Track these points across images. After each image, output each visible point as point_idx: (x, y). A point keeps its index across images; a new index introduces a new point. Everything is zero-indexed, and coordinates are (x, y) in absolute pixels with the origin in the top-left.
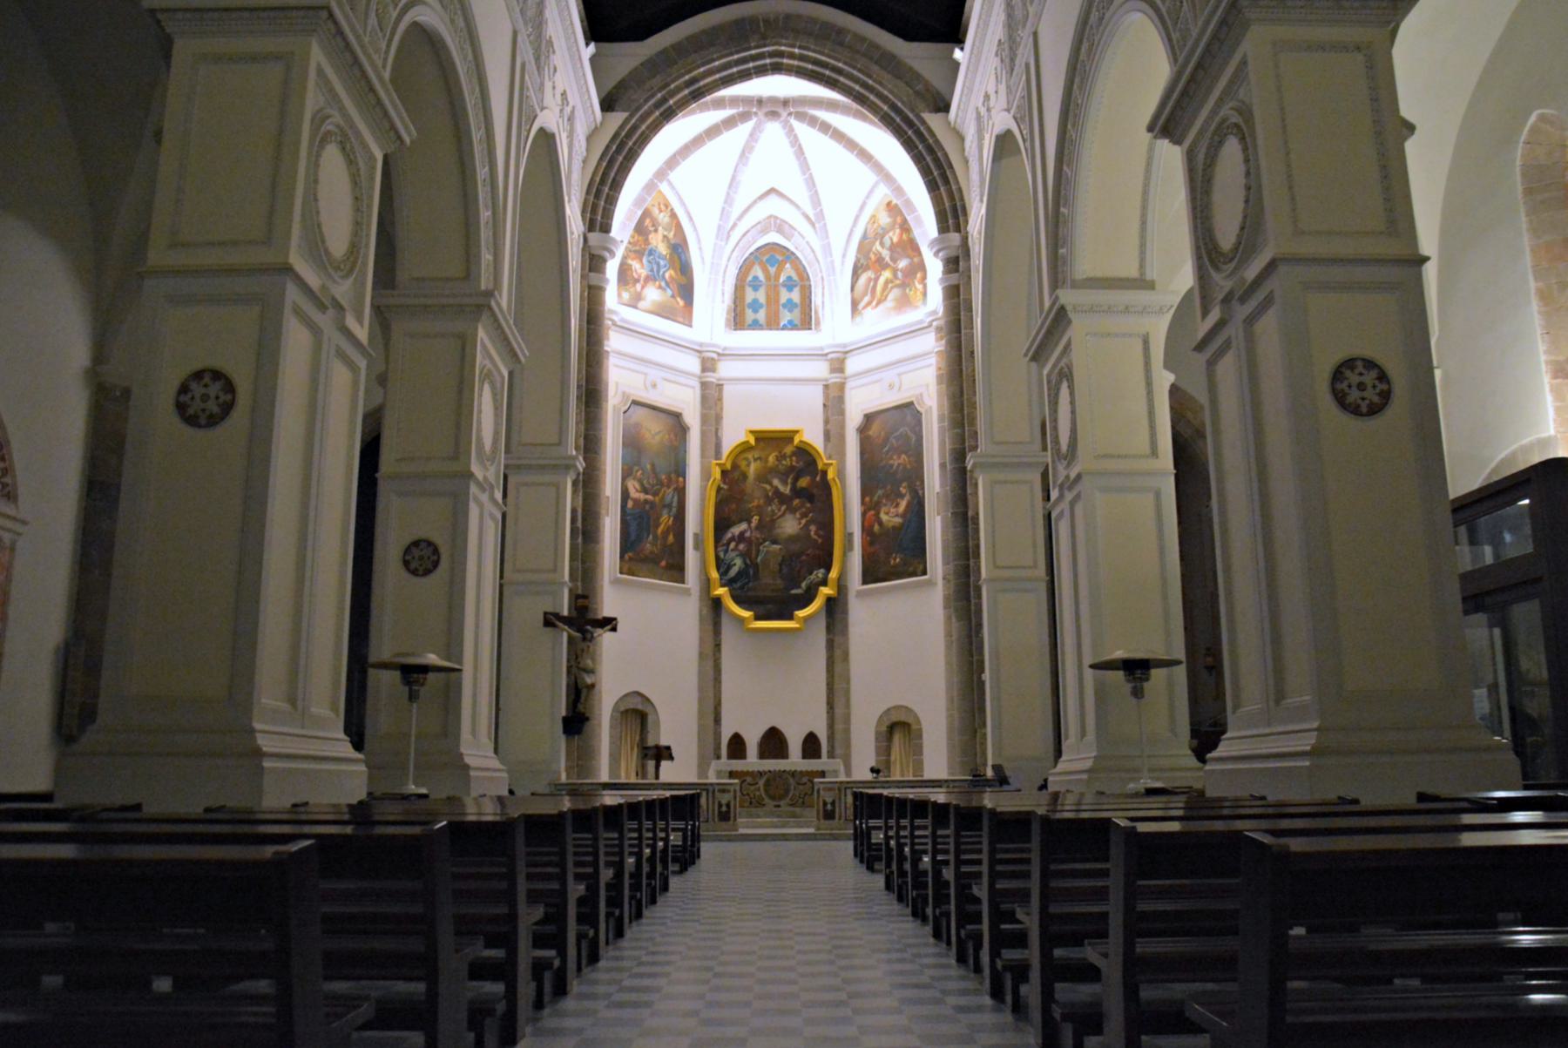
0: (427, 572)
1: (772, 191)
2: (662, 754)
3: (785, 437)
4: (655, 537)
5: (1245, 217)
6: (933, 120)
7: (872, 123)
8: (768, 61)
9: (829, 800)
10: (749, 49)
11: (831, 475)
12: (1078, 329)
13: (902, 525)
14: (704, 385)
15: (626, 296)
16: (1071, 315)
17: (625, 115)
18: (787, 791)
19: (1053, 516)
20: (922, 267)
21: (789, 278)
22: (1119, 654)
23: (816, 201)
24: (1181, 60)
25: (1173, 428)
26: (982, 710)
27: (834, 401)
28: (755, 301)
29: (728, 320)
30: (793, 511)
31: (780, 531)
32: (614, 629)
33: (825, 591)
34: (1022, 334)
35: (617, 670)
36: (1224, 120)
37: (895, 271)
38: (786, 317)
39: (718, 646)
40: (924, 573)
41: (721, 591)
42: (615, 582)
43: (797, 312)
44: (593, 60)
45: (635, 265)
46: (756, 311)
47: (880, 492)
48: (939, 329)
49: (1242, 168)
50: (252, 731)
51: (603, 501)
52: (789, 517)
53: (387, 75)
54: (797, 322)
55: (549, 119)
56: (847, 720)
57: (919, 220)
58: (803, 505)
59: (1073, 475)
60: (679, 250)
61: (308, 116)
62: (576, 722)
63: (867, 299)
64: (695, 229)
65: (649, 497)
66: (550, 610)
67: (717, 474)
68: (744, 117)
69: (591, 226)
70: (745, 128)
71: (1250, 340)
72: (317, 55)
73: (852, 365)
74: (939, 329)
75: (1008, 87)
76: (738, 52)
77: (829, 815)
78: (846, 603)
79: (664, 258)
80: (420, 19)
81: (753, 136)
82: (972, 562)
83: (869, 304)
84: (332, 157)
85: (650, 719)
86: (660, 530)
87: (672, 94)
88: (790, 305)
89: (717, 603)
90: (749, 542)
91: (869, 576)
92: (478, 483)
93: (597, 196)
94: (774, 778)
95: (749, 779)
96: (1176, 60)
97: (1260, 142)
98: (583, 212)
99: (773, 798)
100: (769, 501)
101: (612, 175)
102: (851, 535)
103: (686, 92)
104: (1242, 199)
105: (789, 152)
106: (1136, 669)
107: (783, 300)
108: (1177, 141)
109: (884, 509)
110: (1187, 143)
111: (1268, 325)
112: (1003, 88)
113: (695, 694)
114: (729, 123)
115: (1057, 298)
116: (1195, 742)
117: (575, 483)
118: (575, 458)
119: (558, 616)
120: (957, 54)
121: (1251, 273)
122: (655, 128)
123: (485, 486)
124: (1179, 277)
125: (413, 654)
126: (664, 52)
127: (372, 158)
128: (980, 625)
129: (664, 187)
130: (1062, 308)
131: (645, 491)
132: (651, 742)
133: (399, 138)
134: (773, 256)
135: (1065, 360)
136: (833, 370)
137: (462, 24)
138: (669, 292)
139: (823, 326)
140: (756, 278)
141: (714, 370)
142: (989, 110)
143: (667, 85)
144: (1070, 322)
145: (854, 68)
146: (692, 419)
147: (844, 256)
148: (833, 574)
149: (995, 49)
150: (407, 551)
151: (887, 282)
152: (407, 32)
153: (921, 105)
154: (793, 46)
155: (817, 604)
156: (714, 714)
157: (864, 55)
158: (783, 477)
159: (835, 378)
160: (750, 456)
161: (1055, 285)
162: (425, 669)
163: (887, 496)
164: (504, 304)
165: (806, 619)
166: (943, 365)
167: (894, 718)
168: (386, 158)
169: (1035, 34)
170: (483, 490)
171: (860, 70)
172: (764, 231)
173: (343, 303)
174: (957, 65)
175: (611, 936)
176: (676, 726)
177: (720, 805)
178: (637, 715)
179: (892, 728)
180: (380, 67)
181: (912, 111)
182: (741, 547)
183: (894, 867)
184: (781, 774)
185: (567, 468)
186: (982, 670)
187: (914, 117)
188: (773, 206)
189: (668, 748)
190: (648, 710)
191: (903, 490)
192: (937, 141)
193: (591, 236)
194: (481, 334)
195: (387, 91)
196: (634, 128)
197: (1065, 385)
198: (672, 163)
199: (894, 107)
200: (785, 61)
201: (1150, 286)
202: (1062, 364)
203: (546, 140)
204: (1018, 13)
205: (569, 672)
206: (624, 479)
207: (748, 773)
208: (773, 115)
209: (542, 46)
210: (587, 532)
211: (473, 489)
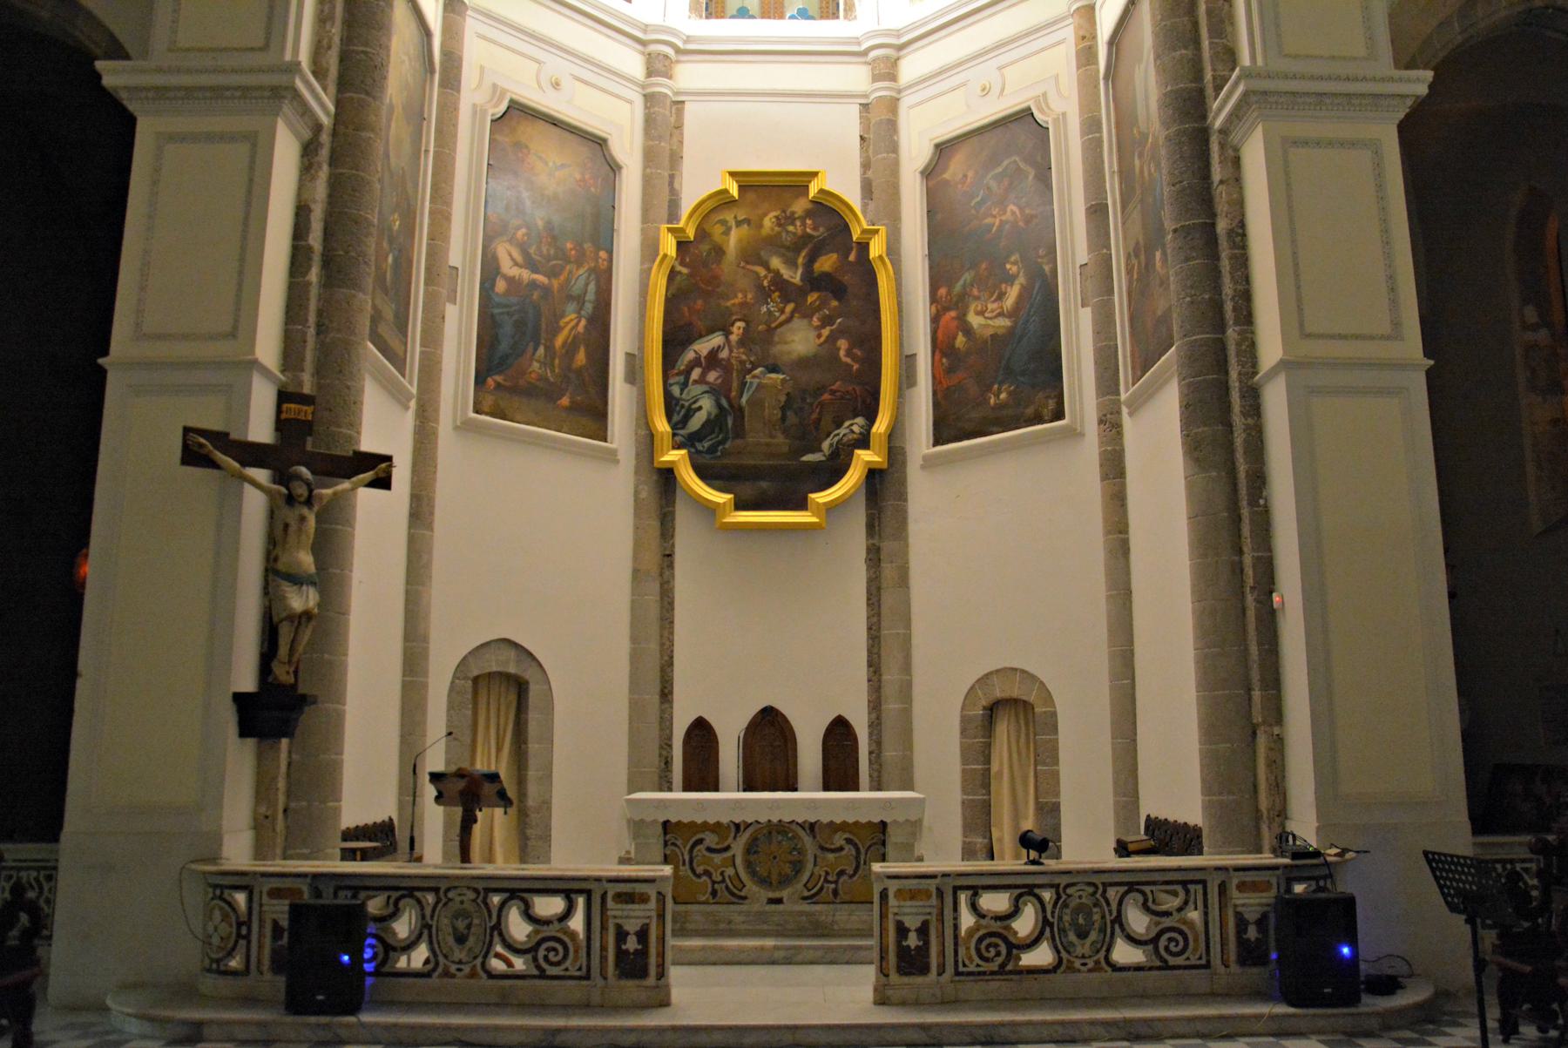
3: (796, 183)
4: (550, 349)
9: (912, 923)
11: (876, 249)
13: (1011, 332)
14: (650, 99)
18: (798, 867)
27: (880, 129)
30: (808, 316)
33: (865, 457)
40: (1059, 415)
41: (675, 457)
42: (465, 427)
47: (967, 277)
52: (797, 323)
58: (824, 303)
67: (669, 246)
73: (912, 67)
77: (912, 962)
78: (903, 482)
82: (1232, 333)
85: (534, 690)
86: (559, 340)
89: (667, 476)
90: (726, 367)
91: (941, 435)
94: (769, 838)
95: (711, 840)
99: (764, 882)
100: (764, 294)
102: (911, 358)
113: (623, 647)
146: (628, 149)
148: (881, 426)
155: (851, 480)
159: (882, 90)
160: (729, 216)
165: (831, 508)
177: (621, 935)
179: (992, 710)
182: (712, 376)
184: (779, 830)
190: (529, 674)
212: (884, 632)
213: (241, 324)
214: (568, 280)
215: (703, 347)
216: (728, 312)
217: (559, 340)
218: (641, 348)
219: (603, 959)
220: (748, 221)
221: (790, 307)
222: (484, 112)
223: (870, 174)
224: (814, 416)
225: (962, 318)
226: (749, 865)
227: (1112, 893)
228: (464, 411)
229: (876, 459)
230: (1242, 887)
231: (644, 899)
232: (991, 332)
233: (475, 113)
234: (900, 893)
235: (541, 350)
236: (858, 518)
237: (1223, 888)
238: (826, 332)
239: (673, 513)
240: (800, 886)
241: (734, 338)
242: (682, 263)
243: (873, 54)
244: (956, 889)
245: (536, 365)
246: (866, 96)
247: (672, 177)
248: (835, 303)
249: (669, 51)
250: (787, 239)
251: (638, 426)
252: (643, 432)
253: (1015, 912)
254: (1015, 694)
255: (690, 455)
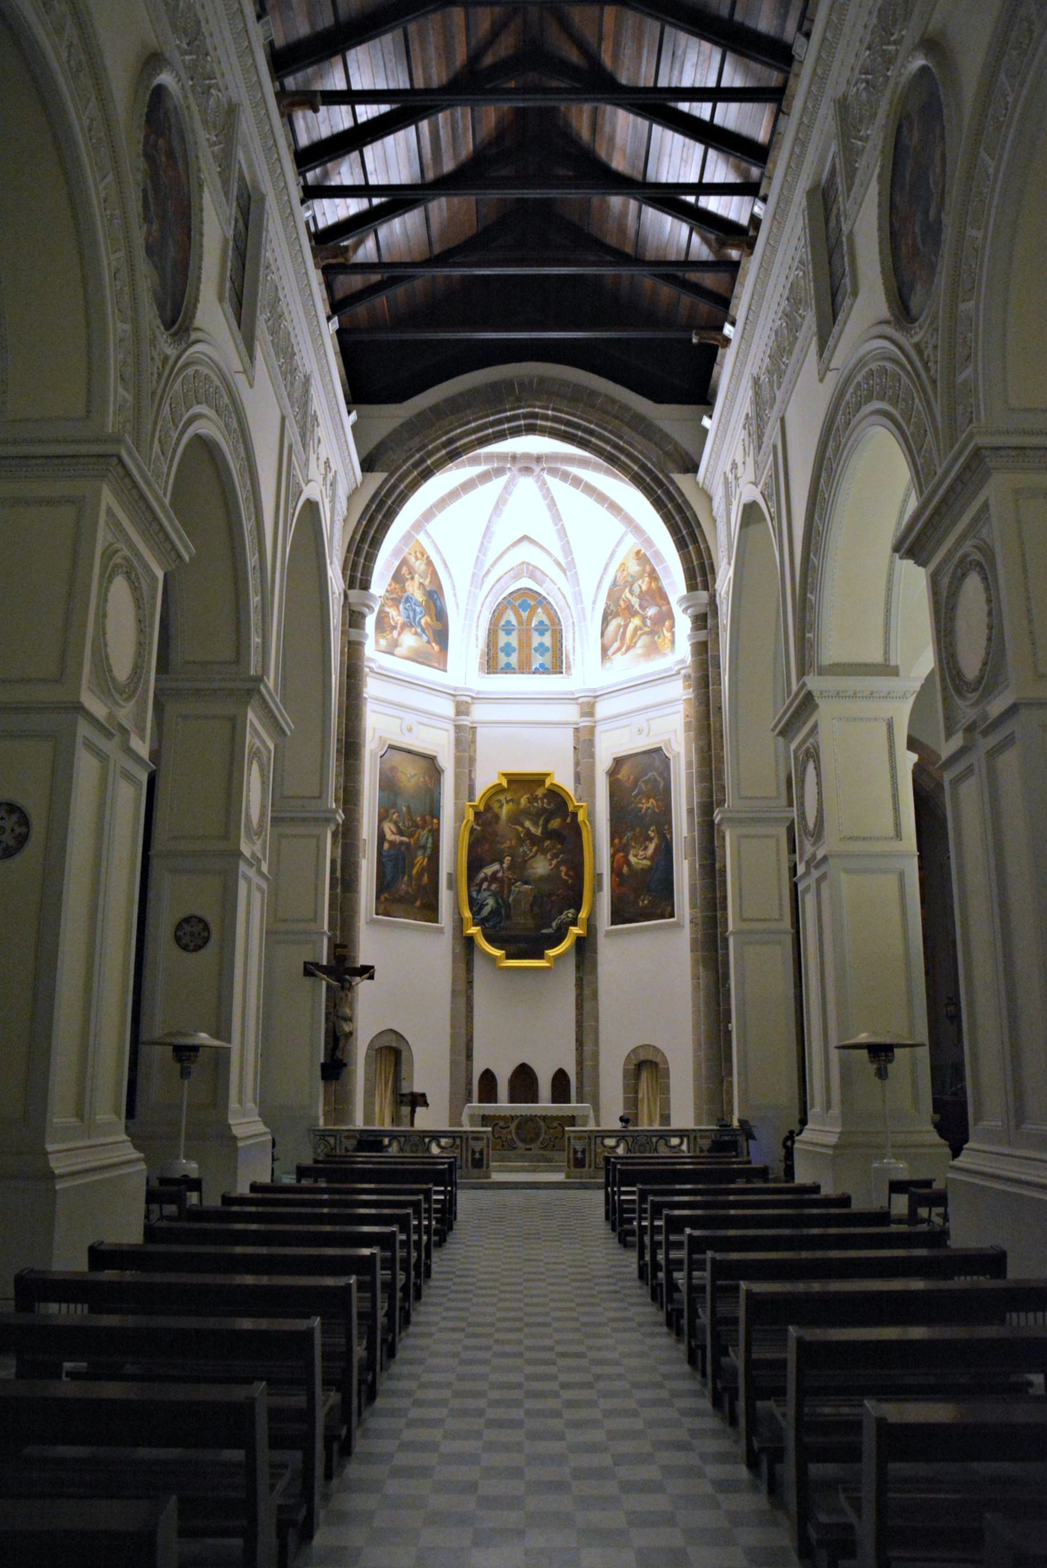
0: (198, 948)
1: (525, 538)
2: (418, 1100)
3: (536, 780)
4: (410, 877)
5: (988, 654)
6: (682, 480)
7: (621, 479)
8: (522, 422)
9: (579, 1148)
10: (505, 411)
11: (581, 817)
12: (826, 713)
13: (650, 868)
14: (458, 728)
15: (383, 642)
16: (818, 700)
17: (385, 475)
18: (538, 1135)
19: (800, 888)
20: (670, 615)
21: (541, 623)
22: (863, 1037)
23: (567, 550)
24: (926, 492)
25: (914, 781)
26: (729, 1060)
27: (584, 745)
28: (508, 645)
29: (481, 664)
30: (543, 851)
31: (531, 871)
32: (371, 977)
33: (575, 930)
34: (769, 712)
35: (371, 1012)
36: (966, 556)
37: (644, 619)
38: (537, 660)
39: (470, 983)
41: (474, 930)
42: (372, 922)
43: (549, 655)
44: (354, 427)
45: (392, 612)
46: (508, 655)
47: (629, 834)
48: (687, 677)
49: (983, 597)
50: (46, 1154)
51: (361, 845)
53: (167, 501)
54: (548, 665)
55: (313, 491)
56: (596, 1055)
57: (666, 570)
58: (554, 847)
59: (819, 856)
60: (434, 597)
61: (99, 549)
62: (334, 1068)
63: (616, 645)
64: (450, 576)
65: (405, 839)
66: (310, 959)
67: (470, 815)
68: (499, 472)
69: (351, 585)
70: (498, 484)
71: (992, 775)
72: (108, 498)
73: (603, 709)
74: (687, 677)
75: (756, 463)
76: (493, 414)
77: (579, 1163)
79: (420, 605)
80: (201, 431)
81: (507, 489)
83: (619, 649)
84: (120, 587)
86: (415, 871)
87: (430, 454)
88: (542, 649)
89: (470, 940)
90: (501, 881)
91: (618, 917)
92: (246, 860)
93: (358, 553)
96: (921, 492)
97: (1002, 581)
98: (344, 569)
99: (524, 1141)
100: (521, 841)
101: (372, 532)
102: (600, 875)
103: (444, 452)
104: (985, 637)
105: (542, 504)
106: (880, 1053)
107: (535, 644)
108: (922, 563)
109: (632, 852)
110: (933, 565)
111: (1009, 761)
112: (750, 461)
114: (484, 478)
115: (804, 685)
116: (938, 1117)
117: (335, 835)
118: (335, 811)
119: (317, 966)
120: (706, 422)
121: (996, 707)
122: (414, 486)
123: (255, 862)
124: (922, 662)
125: (185, 1035)
126: (421, 414)
127: (155, 578)
128: (726, 977)
129: (421, 537)
130: (809, 696)
131: (400, 833)
132: (405, 1090)
133: (179, 556)
134: (525, 601)
135: (811, 740)
136: (584, 714)
137: (235, 425)
138: (425, 638)
139: (573, 670)
140: (508, 622)
141: (467, 714)
142: (737, 478)
143: (426, 446)
144: (816, 706)
145: (605, 429)
146: (447, 762)
147: (594, 602)
148: (583, 914)
149: (742, 421)
150: (179, 926)
151: (636, 629)
152: (188, 445)
153: (670, 465)
154: (547, 409)
156: (464, 1047)
157: (616, 417)
158: (538, 813)
159: (585, 722)
160: (502, 798)
161: (802, 673)
162: (195, 1049)
163: (635, 838)
164: (271, 684)
165: (557, 958)
166: (692, 712)
167: (643, 1056)
168: (165, 575)
169: (782, 420)
170: (251, 865)
171: (611, 432)
172: (517, 577)
173: (125, 723)
174: (705, 431)
175: (384, 1358)
176: (430, 1072)
177: (474, 1152)
178: (392, 1053)
179: (640, 1066)
180: (161, 495)
181: (662, 471)
182: (494, 887)
183: (647, 1258)
184: (532, 1119)
185: (328, 820)
186: (729, 1020)
187: (664, 476)
188: (526, 553)
189: (423, 1095)
190: (403, 1047)
191: (652, 834)
192: (686, 501)
193: (351, 593)
194: (251, 715)
195: (168, 517)
196: (394, 487)
197: (811, 766)
198: (428, 515)
199: (643, 467)
200: (539, 422)
201: (894, 672)
202: (808, 744)
203: (312, 506)
204: (766, 394)
205: (327, 1019)
206: (380, 822)
207: (500, 1118)
208: (527, 470)
209: (307, 423)
210: (345, 880)
211: (243, 867)
212: (585, 1024)
213: (316, 918)
214: (418, 838)
215: (489, 870)
216: (502, 852)
217: (415, 871)
218: (456, 870)
219: (467, 1161)
220: (512, 800)
221: (535, 849)
222: (376, 754)
223: (579, 769)
224: (549, 908)
225: (626, 856)
226: (517, 1133)
227: (654, 1140)
228: (371, 914)
229: (581, 932)
230: (702, 1137)
231: (482, 1139)
232: (640, 867)
233: (371, 755)
234: (575, 1138)
235: (406, 878)
236: (569, 975)
237: (695, 1138)
238: (554, 862)
239: (472, 960)
240: (539, 1143)
241: (505, 865)
242: (478, 824)
243: (581, 700)
244: (596, 1137)
245: (403, 886)
246: (577, 724)
247: (470, 771)
248: (559, 846)
249: (468, 699)
250: (533, 810)
251: (454, 913)
252: (456, 917)
253: (617, 1145)
254: (650, 1058)
255: (483, 930)
